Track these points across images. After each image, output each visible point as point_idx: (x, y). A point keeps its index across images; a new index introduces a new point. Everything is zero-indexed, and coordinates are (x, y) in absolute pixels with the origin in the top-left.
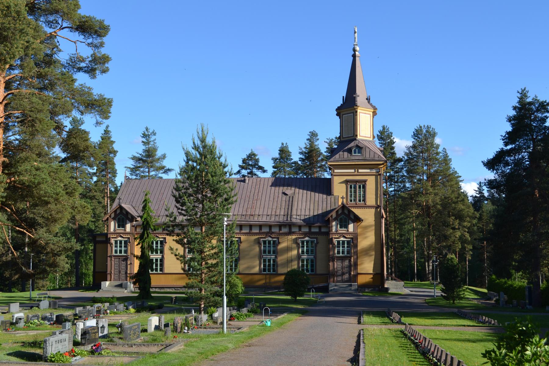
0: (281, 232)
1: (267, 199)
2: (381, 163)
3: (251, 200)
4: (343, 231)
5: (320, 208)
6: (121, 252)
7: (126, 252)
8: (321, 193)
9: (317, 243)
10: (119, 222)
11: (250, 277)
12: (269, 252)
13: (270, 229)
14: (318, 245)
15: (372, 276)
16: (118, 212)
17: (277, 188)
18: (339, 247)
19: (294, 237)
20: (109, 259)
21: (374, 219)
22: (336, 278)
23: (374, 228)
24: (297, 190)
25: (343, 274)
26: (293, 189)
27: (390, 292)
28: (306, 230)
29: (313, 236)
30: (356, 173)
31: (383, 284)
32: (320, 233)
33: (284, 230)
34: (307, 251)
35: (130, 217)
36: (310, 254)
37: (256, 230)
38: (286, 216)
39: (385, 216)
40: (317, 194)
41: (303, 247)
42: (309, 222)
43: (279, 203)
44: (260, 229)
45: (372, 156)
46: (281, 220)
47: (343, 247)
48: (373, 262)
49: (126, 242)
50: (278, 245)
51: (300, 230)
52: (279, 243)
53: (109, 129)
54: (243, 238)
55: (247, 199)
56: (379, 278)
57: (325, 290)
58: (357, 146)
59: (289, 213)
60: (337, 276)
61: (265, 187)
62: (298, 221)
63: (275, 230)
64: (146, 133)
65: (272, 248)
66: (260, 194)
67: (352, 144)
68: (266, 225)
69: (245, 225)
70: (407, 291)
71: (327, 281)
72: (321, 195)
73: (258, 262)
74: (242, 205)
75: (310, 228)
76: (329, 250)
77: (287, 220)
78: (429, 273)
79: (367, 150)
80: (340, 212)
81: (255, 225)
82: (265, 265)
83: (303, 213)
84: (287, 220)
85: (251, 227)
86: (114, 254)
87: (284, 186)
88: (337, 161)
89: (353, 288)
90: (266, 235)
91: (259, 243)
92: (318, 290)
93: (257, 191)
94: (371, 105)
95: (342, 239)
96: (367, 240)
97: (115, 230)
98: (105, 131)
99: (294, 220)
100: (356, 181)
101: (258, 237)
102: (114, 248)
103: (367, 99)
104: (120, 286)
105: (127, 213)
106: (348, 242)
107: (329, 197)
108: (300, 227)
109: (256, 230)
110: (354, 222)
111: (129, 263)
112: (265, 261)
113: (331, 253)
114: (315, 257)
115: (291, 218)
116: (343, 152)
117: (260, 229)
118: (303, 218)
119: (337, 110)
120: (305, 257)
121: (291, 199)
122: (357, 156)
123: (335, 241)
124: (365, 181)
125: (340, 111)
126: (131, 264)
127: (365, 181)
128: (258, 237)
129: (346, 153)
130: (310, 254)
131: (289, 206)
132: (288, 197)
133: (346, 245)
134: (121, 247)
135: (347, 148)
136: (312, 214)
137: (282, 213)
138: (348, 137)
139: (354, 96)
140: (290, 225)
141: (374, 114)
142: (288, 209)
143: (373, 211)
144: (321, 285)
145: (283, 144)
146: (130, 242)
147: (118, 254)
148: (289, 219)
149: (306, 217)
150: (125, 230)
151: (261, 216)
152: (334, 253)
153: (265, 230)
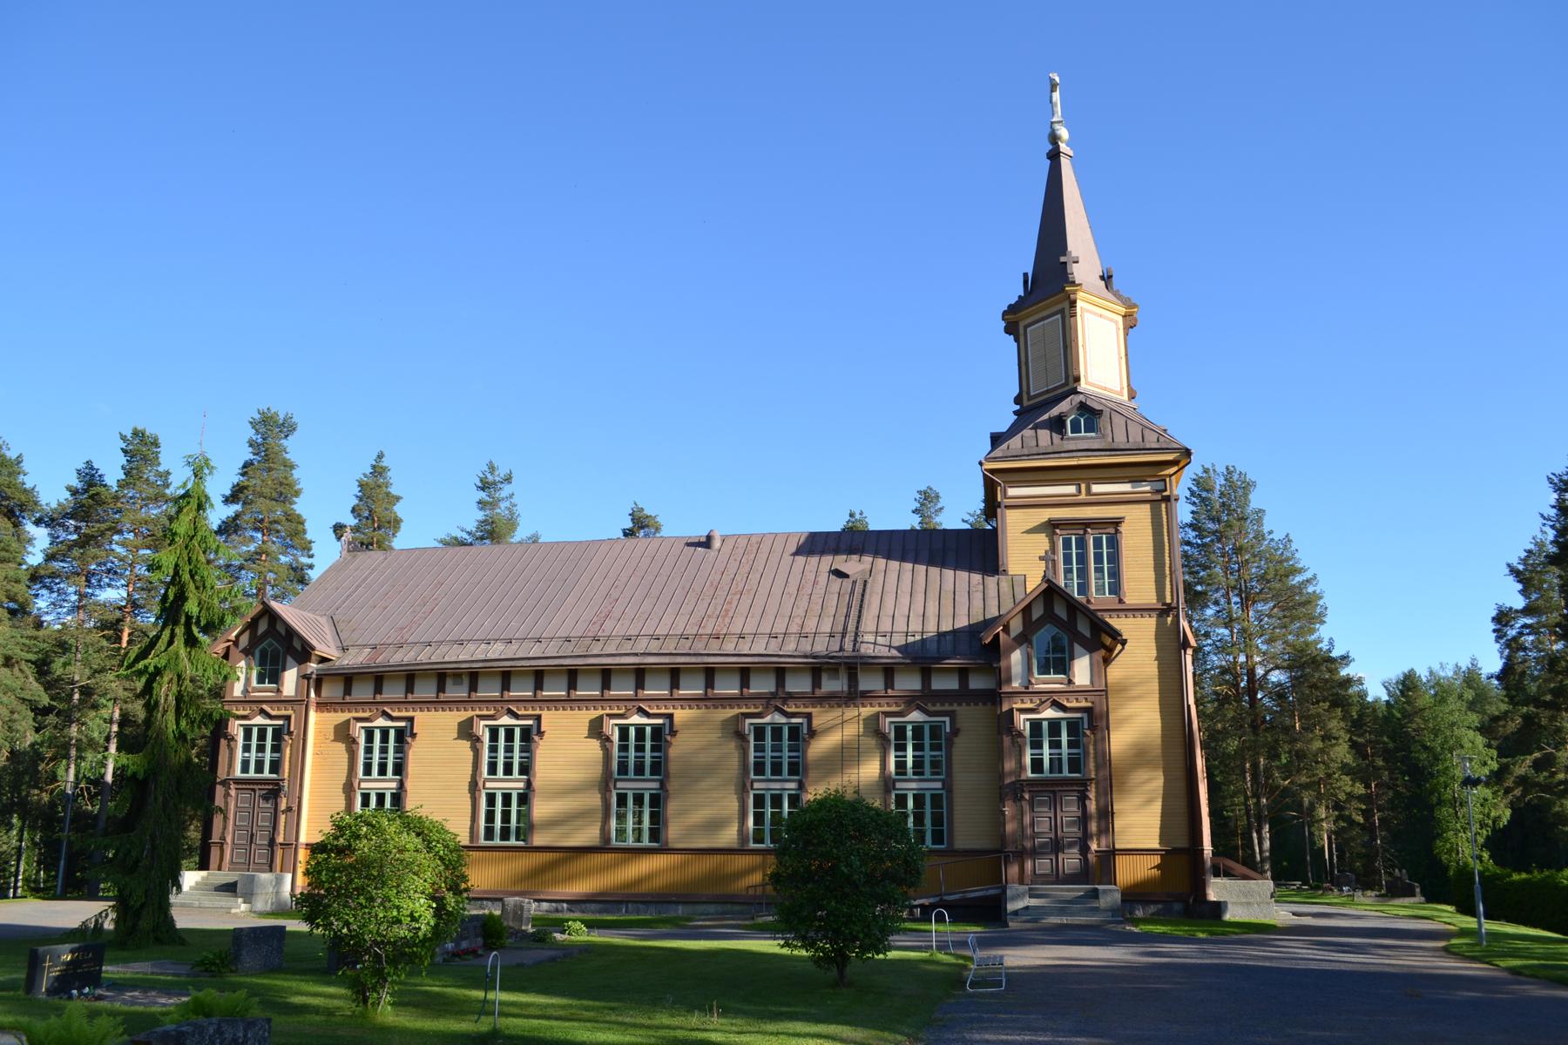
0: (818, 693)
1: (777, 591)
2: (1170, 457)
3: (721, 594)
4: (1049, 682)
5: (962, 611)
6: (259, 767)
7: (276, 766)
8: (962, 568)
9: (955, 732)
10: (262, 663)
11: (709, 863)
12: (777, 769)
13: (780, 682)
14: (956, 740)
15: (1157, 860)
16: (260, 631)
17: (814, 560)
18: (1037, 745)
19: (867, 711)
20: (220, 790)
21: (1154, 653)
22: (1029, 865)
23: (1155, 686)
24: (881, 562)
25: (1057, 846)
26: (868, 559)
27: (1227, 917)
28: (909, 683)
29: (938, 708)
30: (1083, 496)
31: (1200, 888)
32: (962, 695)
33: (830, 685)
34: (918, 764)
35: (297, 644)
36: (927, 775)
37: (727, 687)
38: (838, 637)
39: (1193, 642)
40: (949, 573)
41: (901, 748)
42: (921, 657)
43: (817, 599)
44: (745, 683)
45: (1136, 438)
46: (820, 647)
47: (1055, 745)
48: (1157, 807)
49: (278, 733)
50: (807, 743)
51: (889, 684)
52: (813, 733)
53: (385, 463)
54: (681, 715)
55: (708, 592)
56: (1182, 866)
57: (988, 911)
58: (1084, 408)
59: (851, 627)
60: (1035, 853)
61: (775, 558)
62: (884, 651)
63: (798, 684)
64: (490, 478)
65: (786, 753)
66: (754, 577)
67: (1064, 406)
68: (763, 669)
69: (691, 670)
70: (1282, 915)
71: (997, 879)
72: (963, 575)
73: (734, 805)
74: (686, 609)
75: (926, 674)
76: (1000, 758)
77: (841, 649)
78: (1263, 860)
79: (1119, 421)
80: (1037, 613)
81: (727, 669)
82: (759, 818)
83: (901, 625)
84: (841, 649)
85: (710, 674)
86: (238, 773)
87: (836, 551)
88: (1016, 457)
89: (1104, 902)
90: (767, 707)
91: (740, 736)
92: (963, 912)
93: (745, 569)
94: (1117, 295)
95: (1050, 713)
96: (1136, 723)
97: (246, 691)
98: (374, 467)
99: (867, 650)
100: (1086, 524)
101: (736, 711)
102: (239, 755)
103: (1102, 278)
104: (230, 888)
105: (291, 633)
106: (1074, 727)
107: (991, 581)
108: (889, 672)
109: (727, 687)
110: (1092, 646)
111: (283, 806)
112: (759, 802)
113: (1009, 765)
114: (948, 786)
115: (855, 641)
116: (1035, 428)
117: (745, 683)
118: (899, 640)
119: (1005, 313)
120: (910, 787)
121: (859, 589)
122: (1086, 439)
123: (1022, 722)
124: (1116, 523)
125: (1014, 320)
126: (289, 809)
127: (1116, 523)
128: (736, 711)
129: (1044, 435)
130: (927, 775)
131: (849, 607)
132: (847, 583)
133: (1064, 738)
134: (261, 749)
135: (1046, 417)
136: (931, 628)
137: (826, 627)
138: (1047, 392)
139: (1062, 259)
140: (853, 666)
141: (1130, 323)
142: (847, 616)
143: (1150, 623)
144: (975, 892)
145: (852, 515)
146: (290, 733)
147: (252, 774)
148: (848, 646)
149: (911, 639)
150: (279, 691)
151: (749, 639)
152: (1021, 767)
153: (762, 685)
